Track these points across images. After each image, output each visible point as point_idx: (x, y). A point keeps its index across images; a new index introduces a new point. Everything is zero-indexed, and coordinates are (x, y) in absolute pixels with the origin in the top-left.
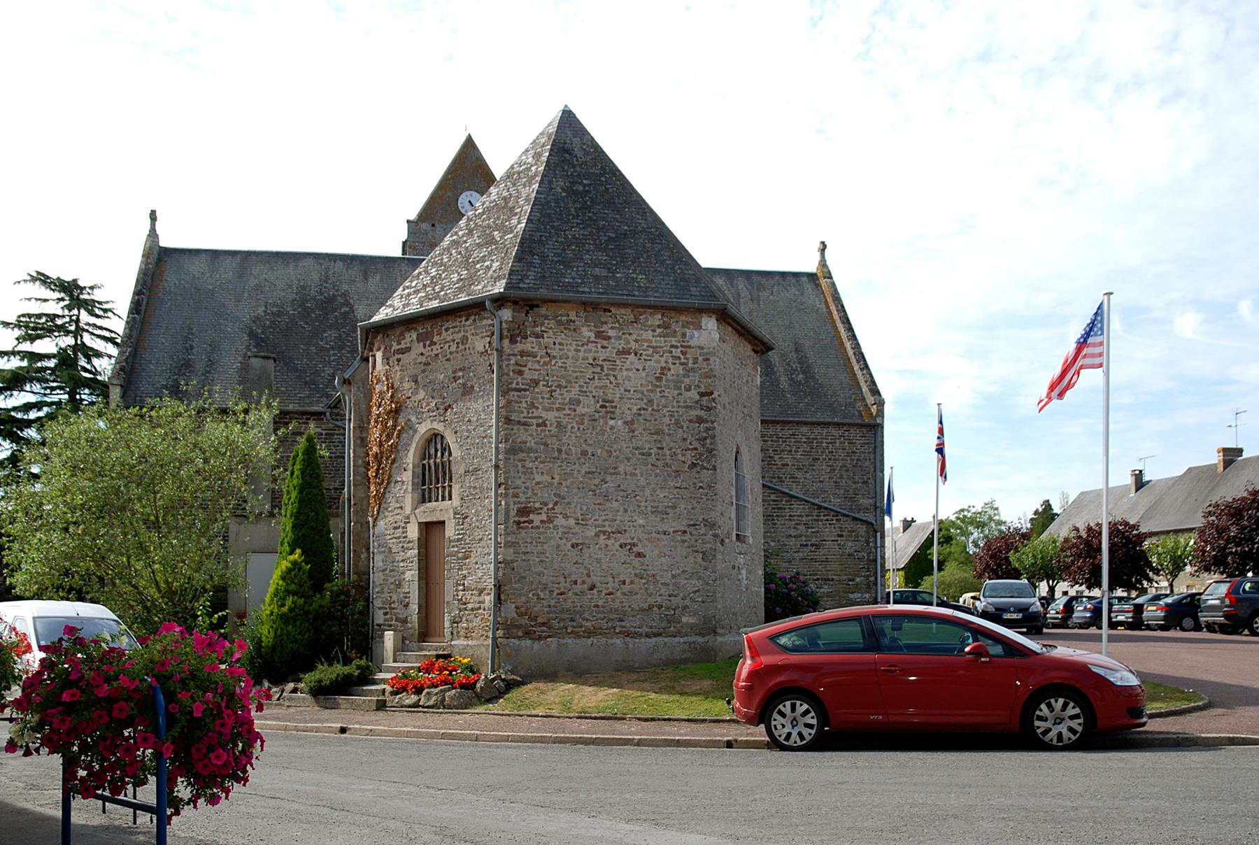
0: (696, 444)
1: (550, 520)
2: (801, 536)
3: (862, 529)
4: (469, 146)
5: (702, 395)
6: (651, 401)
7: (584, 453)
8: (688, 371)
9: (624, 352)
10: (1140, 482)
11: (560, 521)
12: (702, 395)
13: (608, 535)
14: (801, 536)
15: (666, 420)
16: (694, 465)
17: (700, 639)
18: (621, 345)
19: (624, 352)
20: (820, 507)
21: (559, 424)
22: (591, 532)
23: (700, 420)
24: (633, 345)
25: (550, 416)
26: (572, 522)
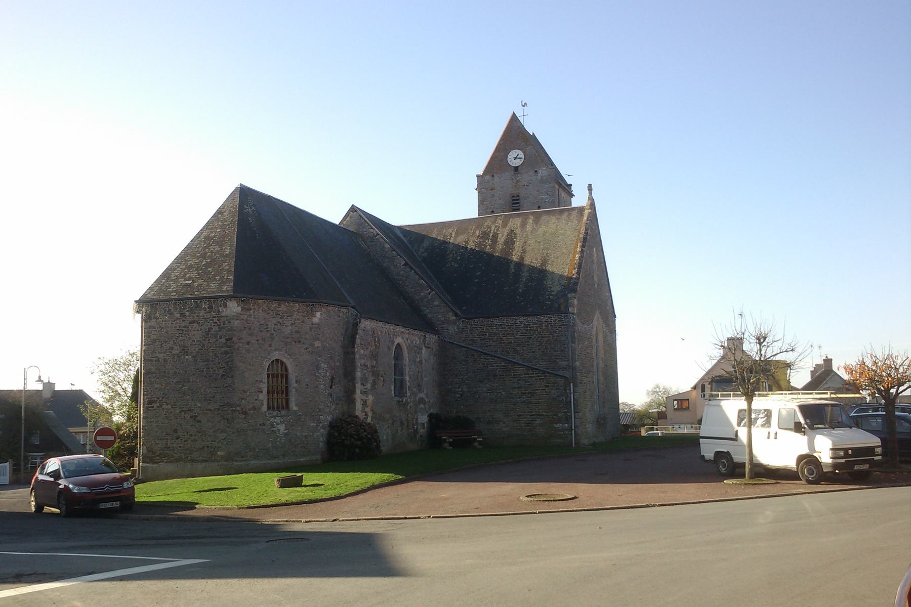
0: (224, 365)
1: (161, 406)
2: (521, 387)
3: (561, 382)
4: (516, 135)
5: (227, 340)
6: (204, 345)
7: (175, 373)
8: (221, 329)
9: (192, 322)
10: (761, 339)
11: (165, 406)
12: (227, 340)
13: (185, 412)
14: (521, 387)
15: (211, 354)
16: (223, 375)
17: (225, 463)
18: (191, 319)
19: (192, 322)
20: (533, 369)
21: (165, 360)
22: (178, 411)
23: (226, 353)
24: (196, 318)
25: (161, 356)
26: (170, 406)
